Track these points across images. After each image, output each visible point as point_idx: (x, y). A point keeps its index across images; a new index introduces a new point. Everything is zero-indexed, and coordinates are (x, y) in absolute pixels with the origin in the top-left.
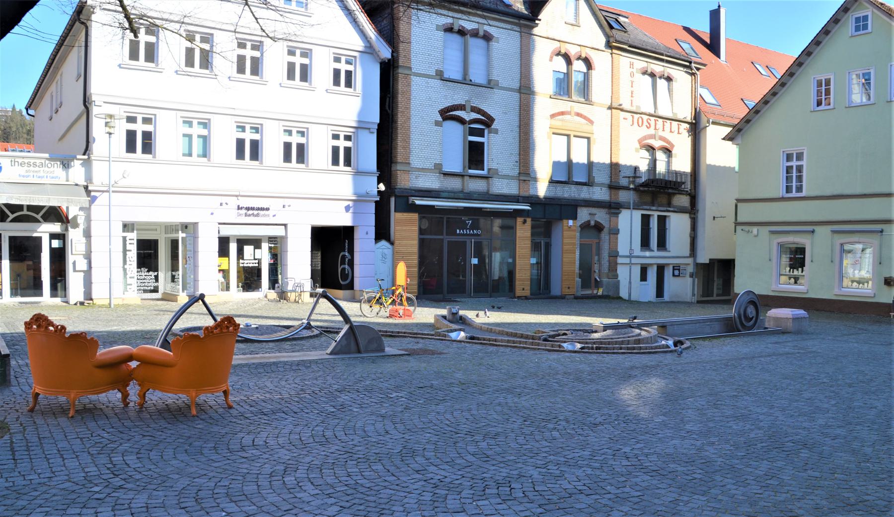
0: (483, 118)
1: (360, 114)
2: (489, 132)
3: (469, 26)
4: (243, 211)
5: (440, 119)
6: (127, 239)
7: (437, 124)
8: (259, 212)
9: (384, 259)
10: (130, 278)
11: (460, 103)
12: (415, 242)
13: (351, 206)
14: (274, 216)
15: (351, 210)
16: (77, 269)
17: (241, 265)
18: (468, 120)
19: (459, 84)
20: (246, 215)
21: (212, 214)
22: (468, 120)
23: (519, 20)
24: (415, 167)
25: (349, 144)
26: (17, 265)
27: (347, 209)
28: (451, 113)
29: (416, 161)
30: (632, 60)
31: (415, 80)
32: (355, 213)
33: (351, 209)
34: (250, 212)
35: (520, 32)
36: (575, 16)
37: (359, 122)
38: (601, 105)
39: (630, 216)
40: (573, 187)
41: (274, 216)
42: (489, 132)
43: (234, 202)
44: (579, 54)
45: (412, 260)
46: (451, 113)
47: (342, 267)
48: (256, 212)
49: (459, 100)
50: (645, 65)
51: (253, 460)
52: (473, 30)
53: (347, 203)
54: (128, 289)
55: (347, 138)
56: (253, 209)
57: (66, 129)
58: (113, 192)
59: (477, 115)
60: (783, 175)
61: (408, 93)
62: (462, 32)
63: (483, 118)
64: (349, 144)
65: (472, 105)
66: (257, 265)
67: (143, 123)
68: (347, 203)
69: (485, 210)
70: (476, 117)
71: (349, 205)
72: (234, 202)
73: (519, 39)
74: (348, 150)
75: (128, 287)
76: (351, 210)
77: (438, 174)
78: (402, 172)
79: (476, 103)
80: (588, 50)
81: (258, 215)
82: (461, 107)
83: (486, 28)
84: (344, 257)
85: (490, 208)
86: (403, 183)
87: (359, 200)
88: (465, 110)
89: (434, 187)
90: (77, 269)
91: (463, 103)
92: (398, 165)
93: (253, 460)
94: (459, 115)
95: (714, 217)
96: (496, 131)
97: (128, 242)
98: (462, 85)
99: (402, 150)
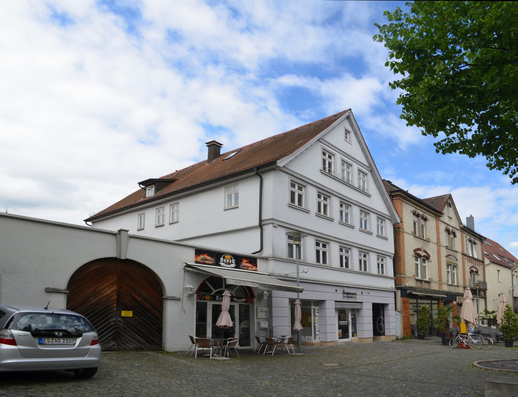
2: (428, 262)
3: (421, 213)
4: (346, 295)
8: (352, 295)
10: (317, 331)
20: (347, 297)
23: (437, 213)
26: (311, 322)
30: (466, 235)
31: (405, 235)
34: (349, 296)
35: (436, 218)
36: (327, 134)
38: (434, 243)
39: (49, 305)
40: (454, 287)
42: (428, 262)
44: (423, 216)
47: (379, 325)
50: (414, 209)
52: (422, 214)
54: (317, 338)
57: (205, 234)
58: (300, 282)
60: (414, 267)
61: (403, 240)
63: (427, 255)
66: (347, 324)
69: (433, 297)
72: (340, 290)
73: (435, 222)
75: (317, 336)
79: (425, 248)
80: (454, 229)
81: (351, 297)
84: (380, 319)
85: (438, 296)
88: (421, 251)
92: (402, 274)
95: (494, 300)
96: (431, 262)
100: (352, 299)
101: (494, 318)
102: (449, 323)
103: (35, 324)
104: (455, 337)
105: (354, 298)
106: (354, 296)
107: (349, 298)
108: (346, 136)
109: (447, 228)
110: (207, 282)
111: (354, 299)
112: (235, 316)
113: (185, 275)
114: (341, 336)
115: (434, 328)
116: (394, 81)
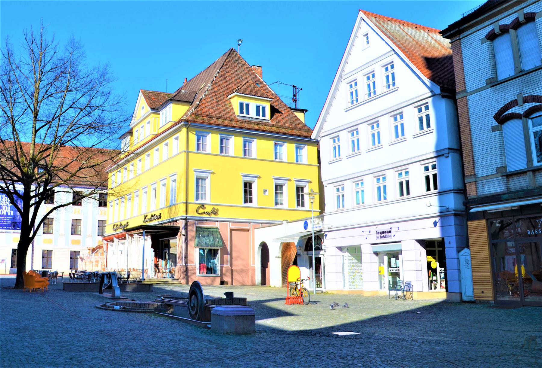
0: (538, 104)
1: (437, 145)
3: (507, 21)
5: (495, 123)
6: (344, 256)
7: (494, 129)
9: (467, 265)
11: (512, 100)
12: (486, 247)
13: (437, 221)
14: (394, 236)
15: (438, 225)
16: (233, 232)
17: (390, 271)
18: (522, 113)
19: (508, 82)
20: (381, 237)
21: (366, 238)
22: (522, 113)
24: (480, 176)
25: (435, 171)
27: (435, 224)
28: (505, 114)
29: (481, 172)
32: (442, 227)
33: (438, 224)
34: (382, 235)
37: (437, 151)
41: (394, 236)
43: (374, 230)
45: (485, 264)
46: (505, 114)
48: (385, 235)
49: (510, 97)
51: (44, 66)
53: (433, 220)
55: (434, 167)
56: (383, 233)
59: (531, 103)
62: (504, 30)
63: (538, 104)
64: (435, 171)
65: (524, 96)
67: (425, 176)
68: (433, 220)
70: (530, 106)
71: (436, 221)
72: (374, 230)
74: (435, 176)
76: (438, 225)
77: (500, 178)
78: (469, 184)
79: (528, 92)
81: (385, 237)
82: (514, 103)
83: (526, 10)
86: (471, 193)
87: (443, 215)
89: (499, 191)
90: (233, 232)
91: (514, 99)
93: (44, 66)
94: (513, 112)
97: (345, 258)
98: (511, 81)
99: (467, 165)
100: (387, 238)
101: (28, 274)
102: (349, 254)
103: (105, 296)
104: (2, 200)
105: (388, 237)
106: (387, 234)
107: (383, 238)
108: (386, 194)
109: (505, 167)
110: (300, 188)
111: (388, 238)
112: (325, 203)
113: (173, 122)
114: (228, 257)
115: (311, 266)
116: (429, 176)
